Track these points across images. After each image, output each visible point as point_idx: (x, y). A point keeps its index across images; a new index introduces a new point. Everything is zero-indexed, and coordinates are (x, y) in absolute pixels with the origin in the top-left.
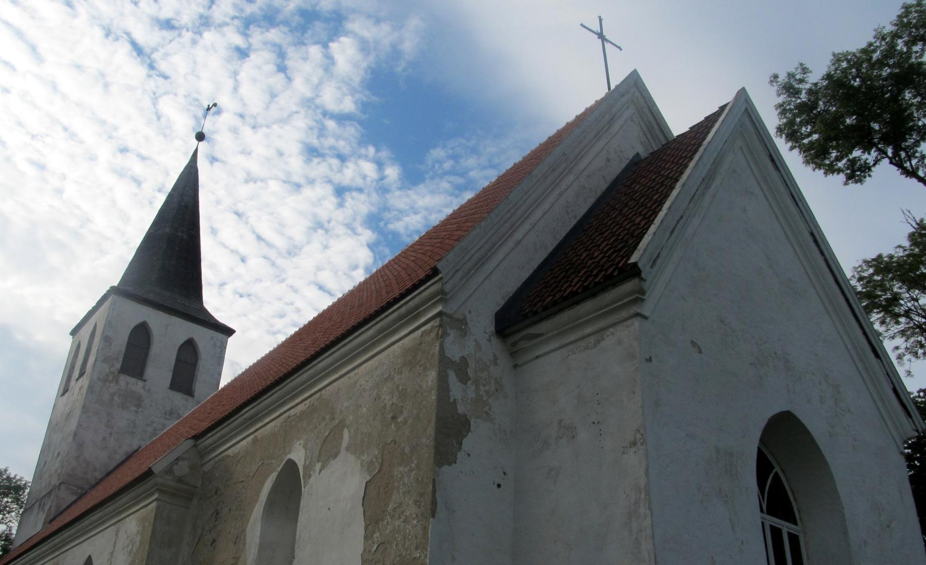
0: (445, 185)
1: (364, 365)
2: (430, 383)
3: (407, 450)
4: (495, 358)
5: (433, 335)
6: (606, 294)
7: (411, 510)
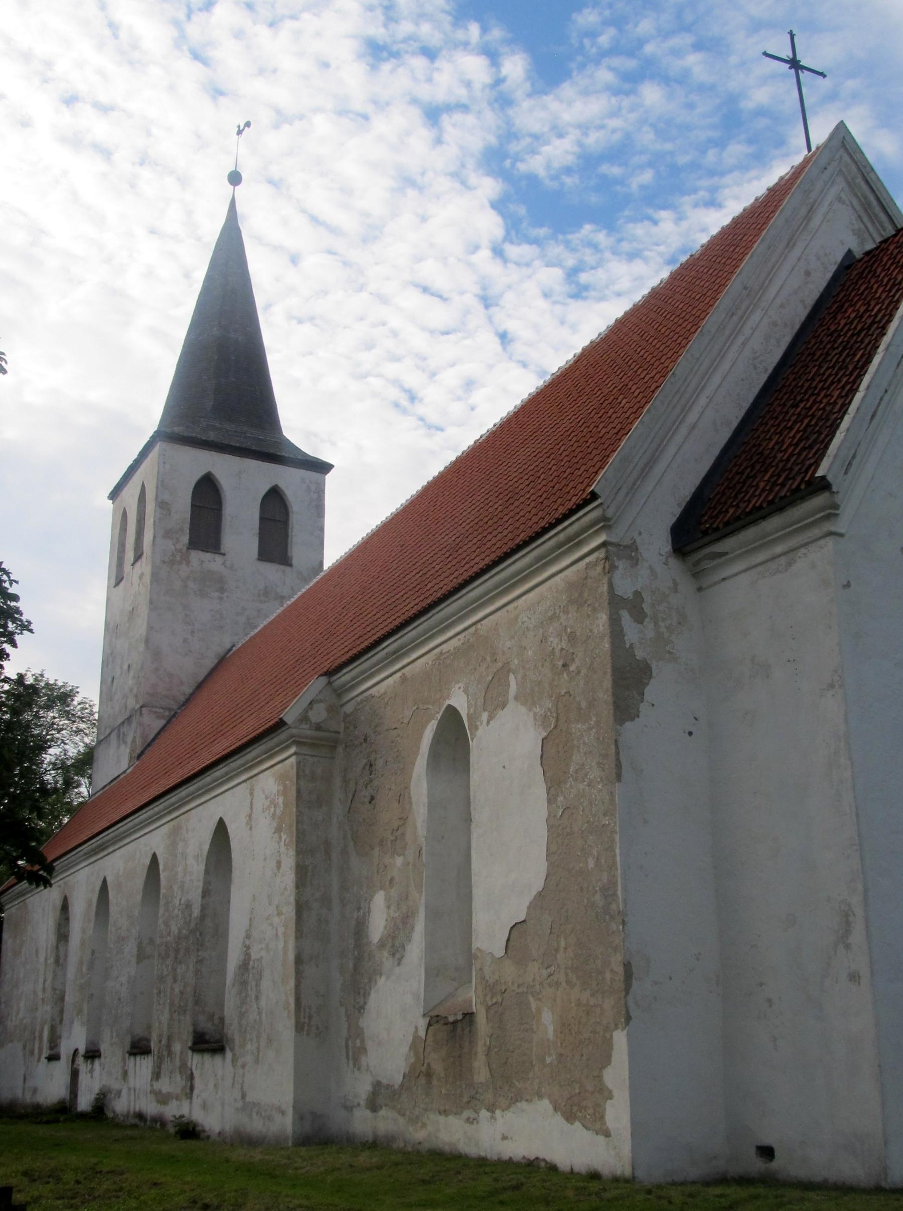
0: (605, 76)
1: (524, 598)
3: (584, 705)
4: (675, 584)
5: (599, 569)
7: (595, 773)
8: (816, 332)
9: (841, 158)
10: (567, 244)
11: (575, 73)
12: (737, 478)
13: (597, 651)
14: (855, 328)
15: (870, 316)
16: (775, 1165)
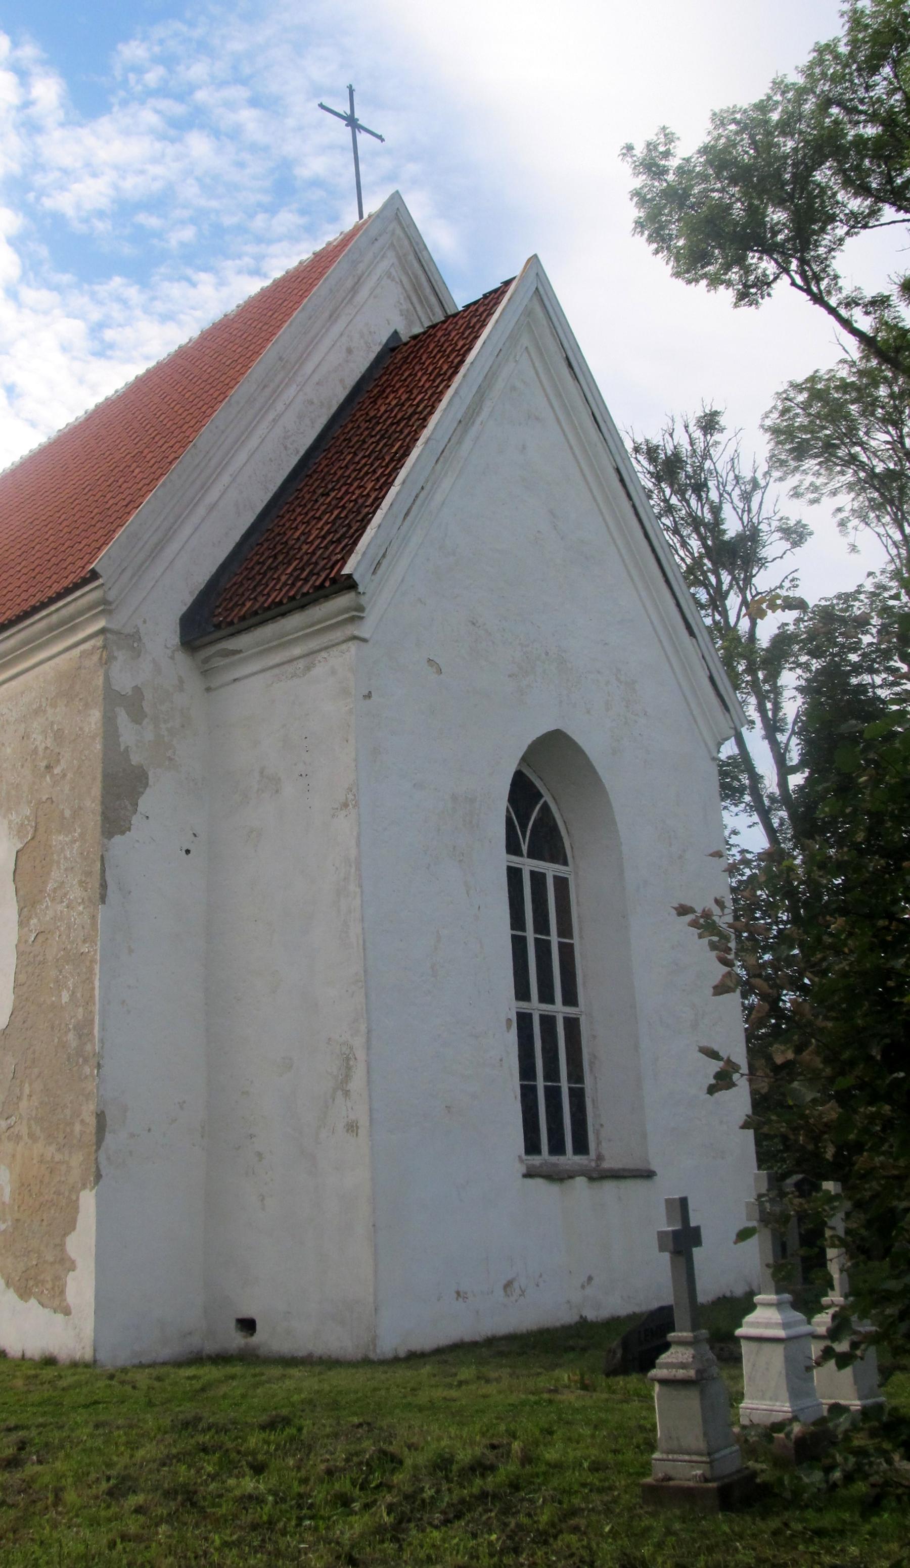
0: (149, 117)
2: (93, 726)
3: (67, 813)
4: (181, 681)
5: (95, 658)
6: (317, 608)
7: (75, 893)
8: (354, 415)
9: (394, 230)
10: (93, 295)
11: (116, 109)
12: (257, 568)
13: (87, 752)
14: (395, 416)
15: (411, 405)
16: (255, 1339)
